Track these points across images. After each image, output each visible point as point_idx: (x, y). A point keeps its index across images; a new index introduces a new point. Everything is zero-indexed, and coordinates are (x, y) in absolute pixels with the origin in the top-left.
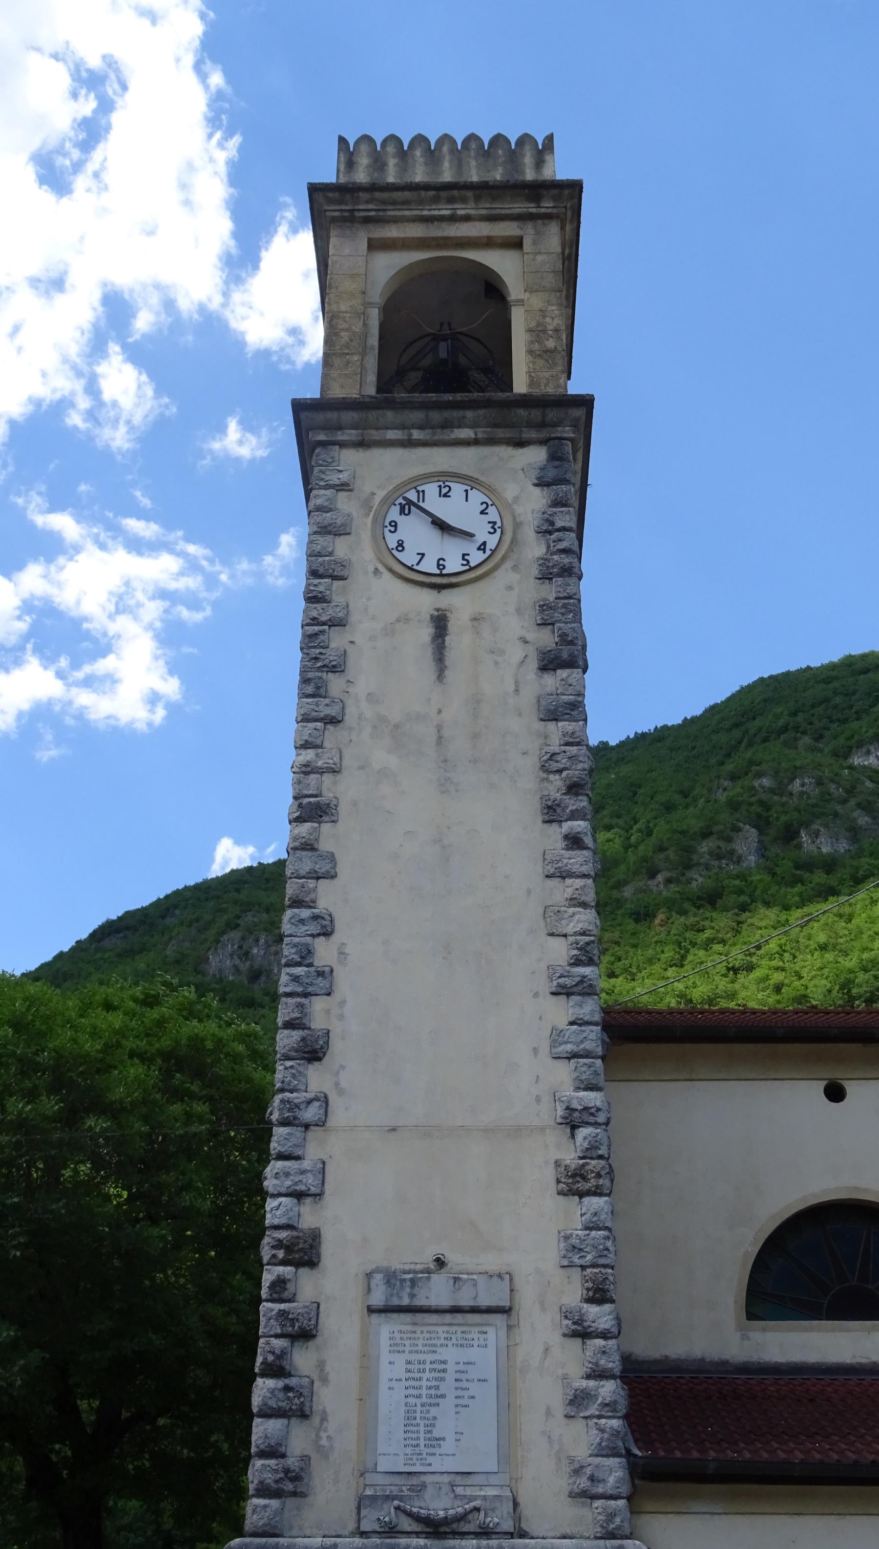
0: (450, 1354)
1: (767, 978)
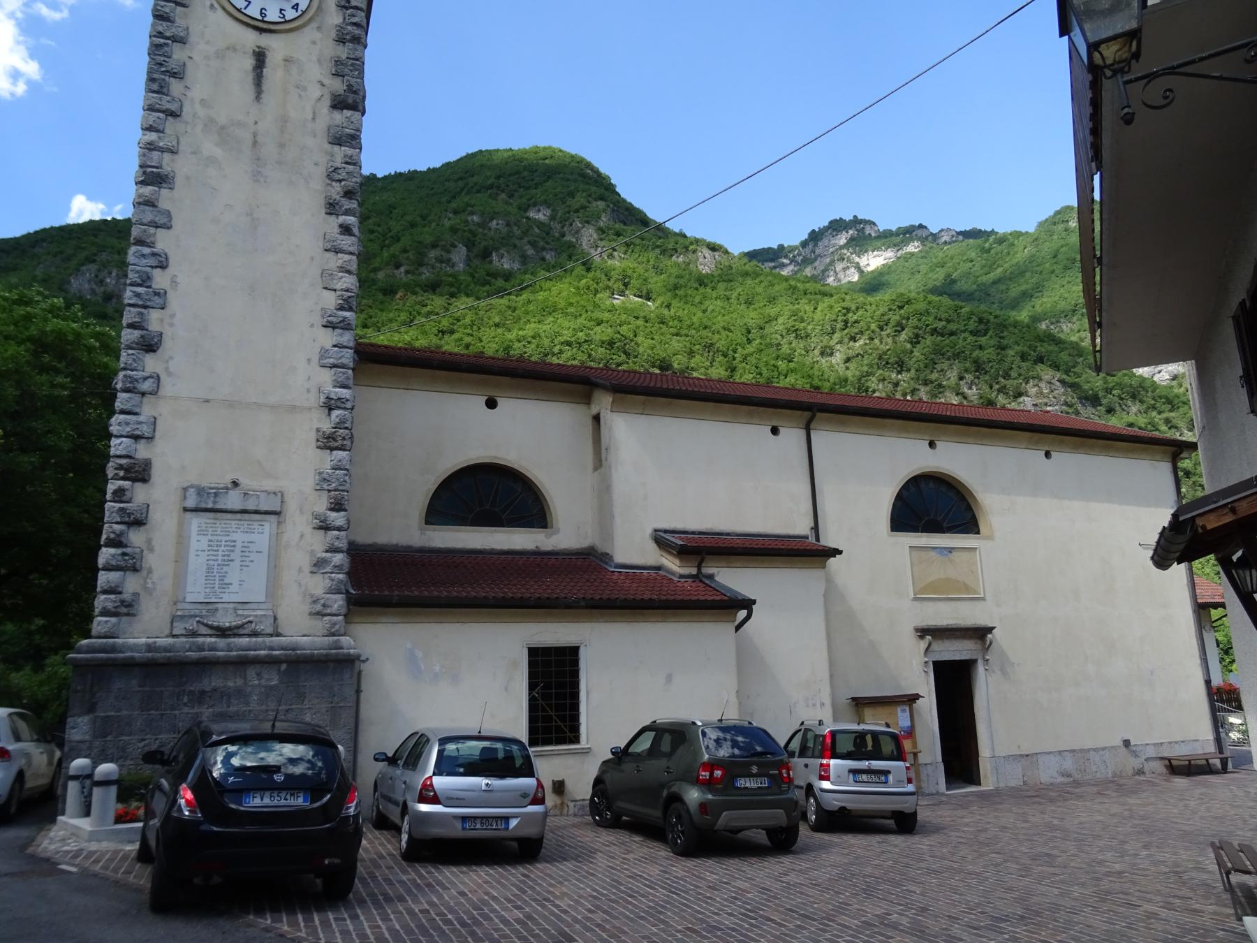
0: (239, 537)
1: (461, 339)
